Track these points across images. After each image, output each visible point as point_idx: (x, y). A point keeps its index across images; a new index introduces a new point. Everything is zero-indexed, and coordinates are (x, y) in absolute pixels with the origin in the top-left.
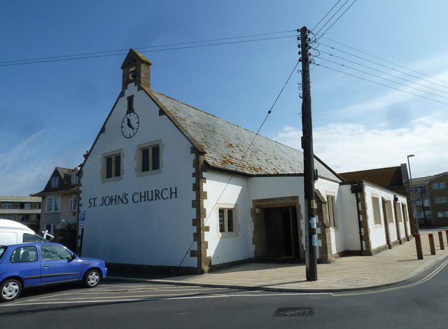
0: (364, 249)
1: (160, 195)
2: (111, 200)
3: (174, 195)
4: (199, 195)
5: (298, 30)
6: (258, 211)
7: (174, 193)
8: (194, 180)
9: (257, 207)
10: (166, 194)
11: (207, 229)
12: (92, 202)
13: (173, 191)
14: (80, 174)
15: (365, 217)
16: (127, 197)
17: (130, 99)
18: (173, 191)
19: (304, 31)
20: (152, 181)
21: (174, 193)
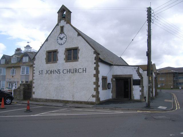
1: (77, 71)
5: (147, 8)
6: (114, 79)
7: (85, 70)
9: (114, 78)
12: (41, 72)
13: (84, 69)
14: (37, 53)
16: (60, 71)
17: (62, 28)
18: (84, 69)
19: (149, 10)
21: (85, 70)
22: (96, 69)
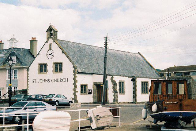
0: (134, 101)
2: (43, 81)
3: (67, 81)
4: (75, 81)
7: (67, 80)
8: (73, 77)
10: (64, 80)
11: (77, 92)
12: (34, 81)
13: (67, 79)
15: (136, 90)
17: (50, 45)
18: (67, 79)
20: (58, 75)
21: (67, 80)
22: (74, 79)
